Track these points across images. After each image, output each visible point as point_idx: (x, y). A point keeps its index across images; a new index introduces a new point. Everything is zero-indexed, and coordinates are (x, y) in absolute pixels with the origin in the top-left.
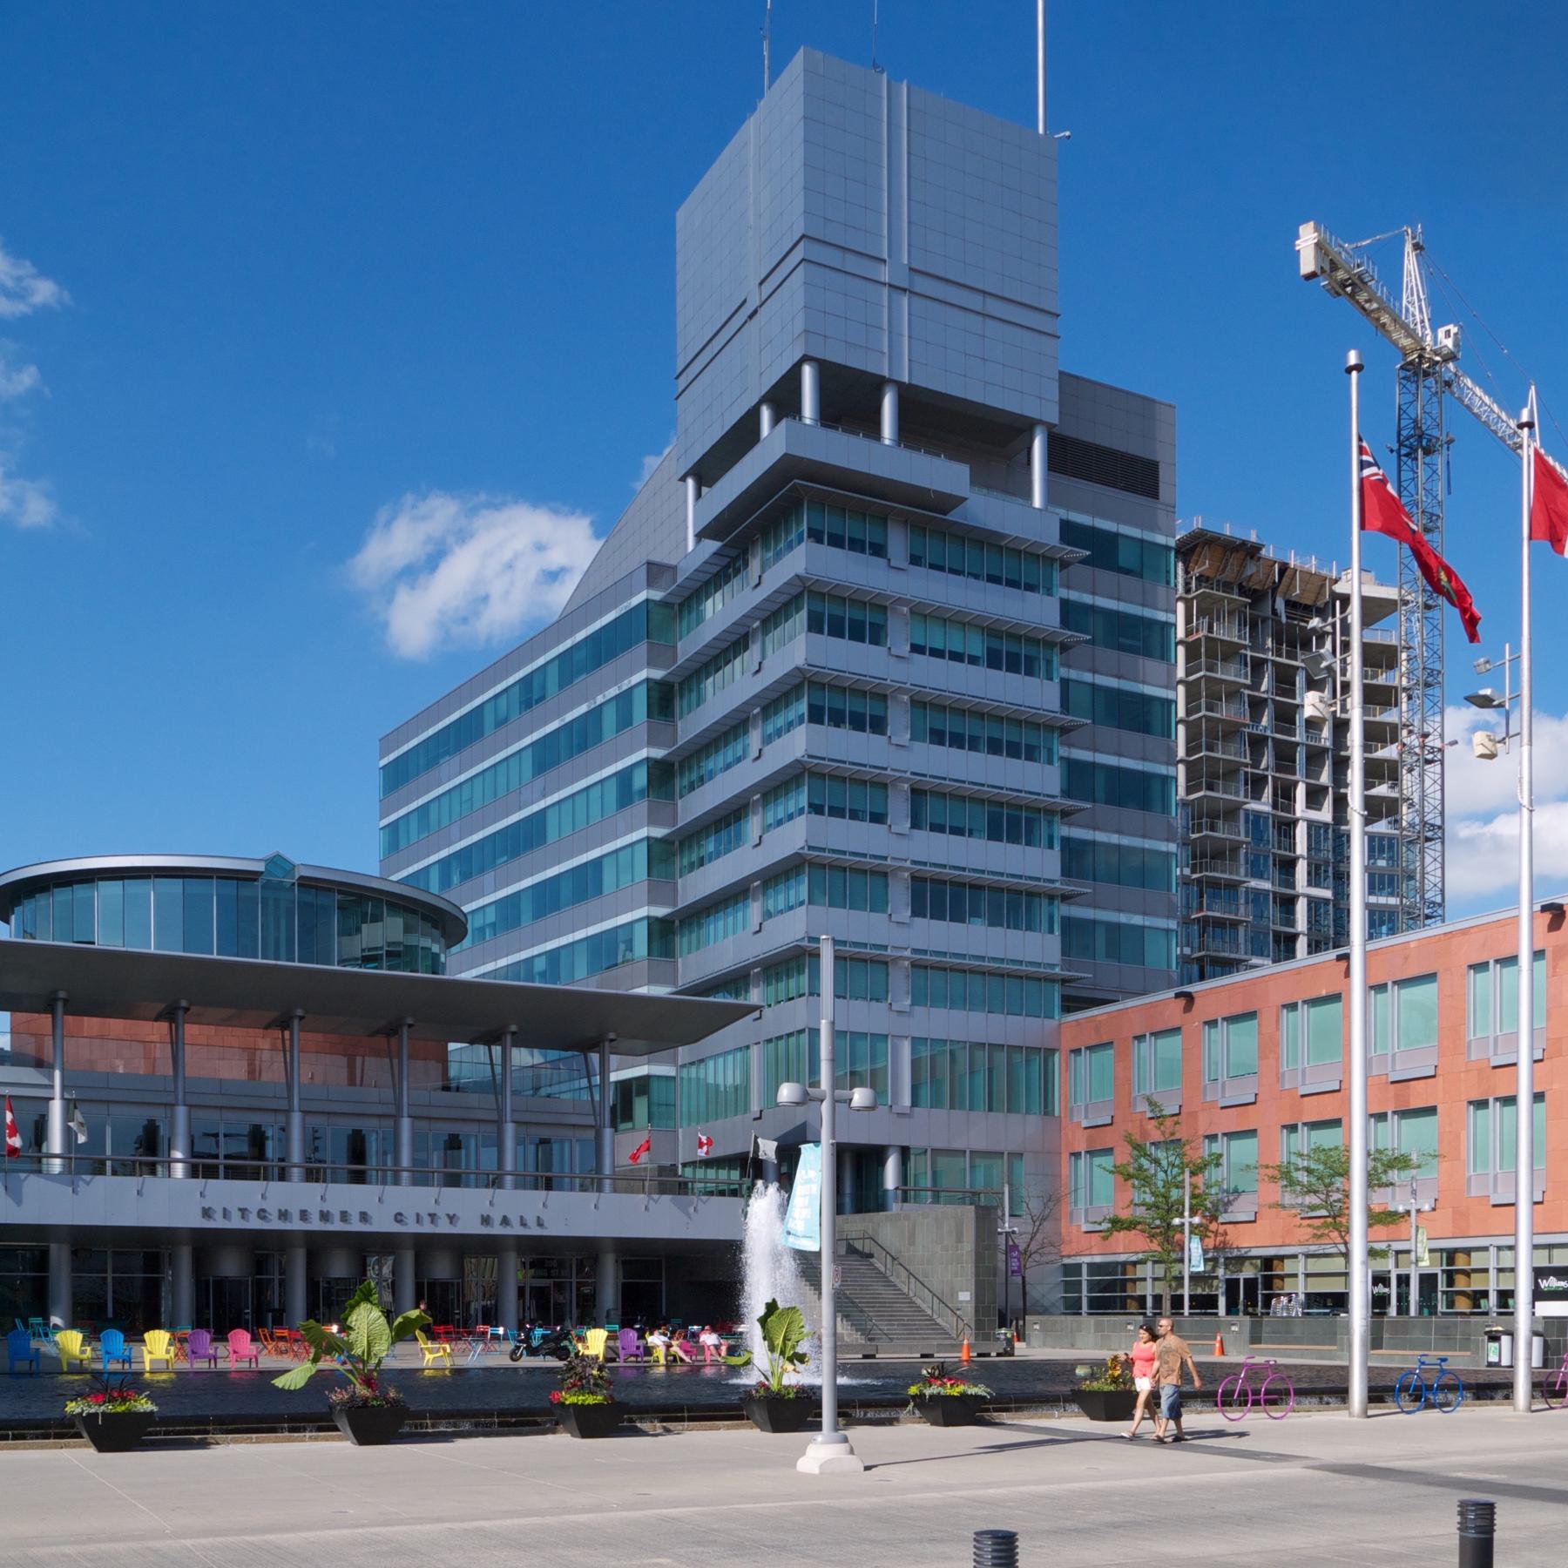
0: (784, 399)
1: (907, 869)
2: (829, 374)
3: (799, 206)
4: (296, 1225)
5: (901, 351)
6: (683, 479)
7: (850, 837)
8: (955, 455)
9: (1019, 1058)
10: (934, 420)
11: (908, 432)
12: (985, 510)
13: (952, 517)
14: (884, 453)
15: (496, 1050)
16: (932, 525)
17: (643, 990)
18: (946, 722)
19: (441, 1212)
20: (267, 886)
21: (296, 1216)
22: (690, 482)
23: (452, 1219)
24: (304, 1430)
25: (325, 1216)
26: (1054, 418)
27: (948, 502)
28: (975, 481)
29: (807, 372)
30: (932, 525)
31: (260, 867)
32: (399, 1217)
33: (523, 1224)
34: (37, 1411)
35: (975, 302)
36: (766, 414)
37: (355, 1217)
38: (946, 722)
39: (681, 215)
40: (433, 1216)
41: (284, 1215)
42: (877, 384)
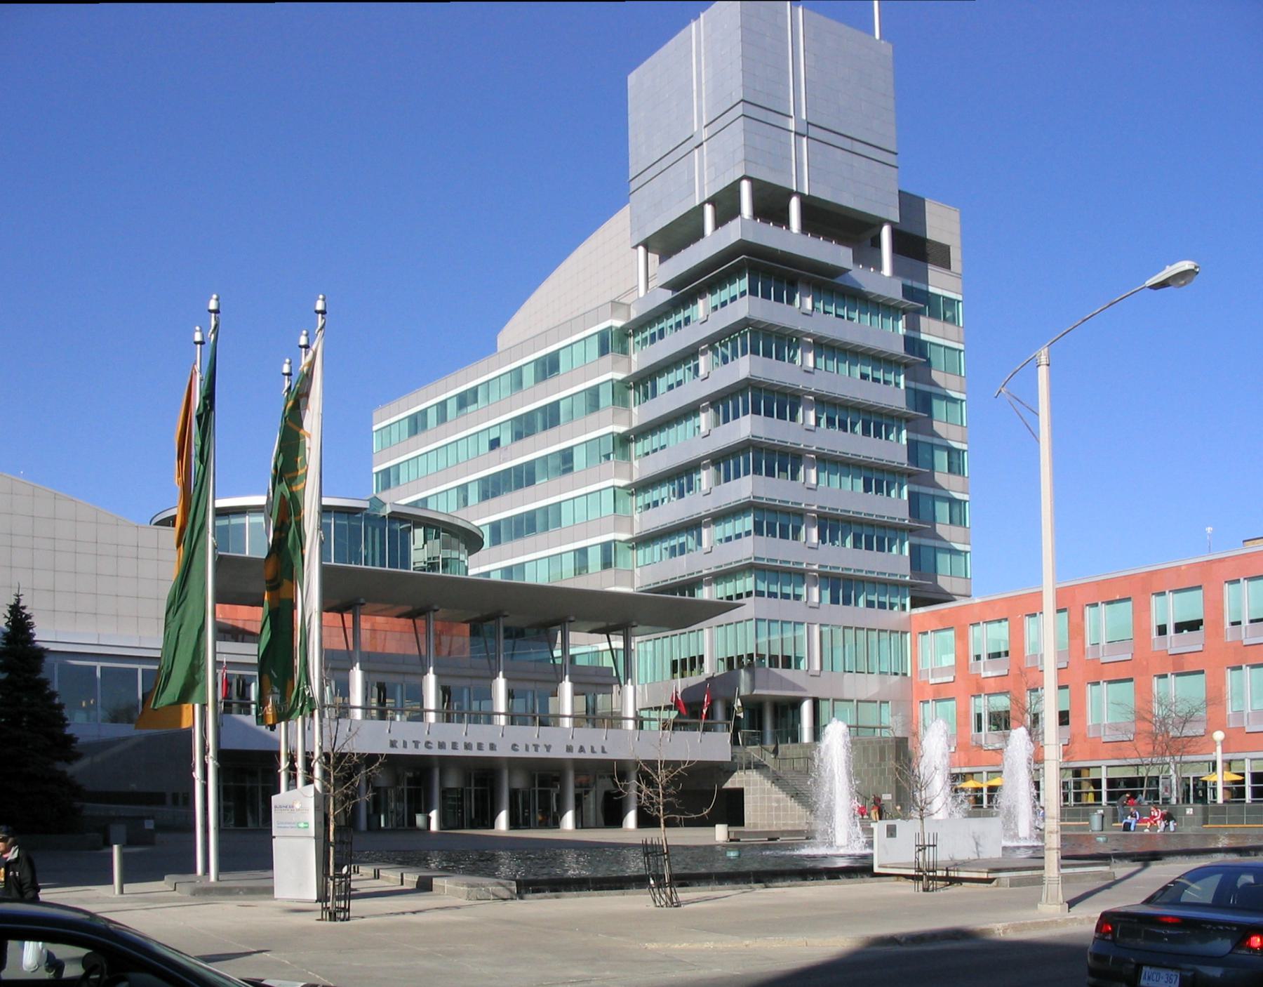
0: (726, 205)
1: (813, 511)
2: (759, 188)
3: (738, 80)
4: (435, 751)
5: (801, 174)
6: (636, 247)
7: (777, 489)
8: (842, 241)
9: (763, 626)
10: (822, 218)
11: (806, 227)
12: (862, 277)
13: (838, 281)
14: (792, 238)
15: (348, 617)
16: (826, 283)
17: (613, 589)
18: (837, 410)
19: (541, 743)
20: (367, 515)
21: (475, 746)
22: (641, 249)
23: (548, 748)
24: (544, 891)
25: (442, 745)
26: (896, 218)
27: (842, 271)
28: (856, 260)
29: (745, 187)
30: (826, 283)
31: (366, 505)
32: (569, 749)
33: (593, 751)
34: (615, 871)
35: (847, 144)
36: (709, 210)
37: (486, 747)
38: (837, 410)
39: (632, 79)
40: (536, 747)
41: (442, 745)
42: (789, 194)
